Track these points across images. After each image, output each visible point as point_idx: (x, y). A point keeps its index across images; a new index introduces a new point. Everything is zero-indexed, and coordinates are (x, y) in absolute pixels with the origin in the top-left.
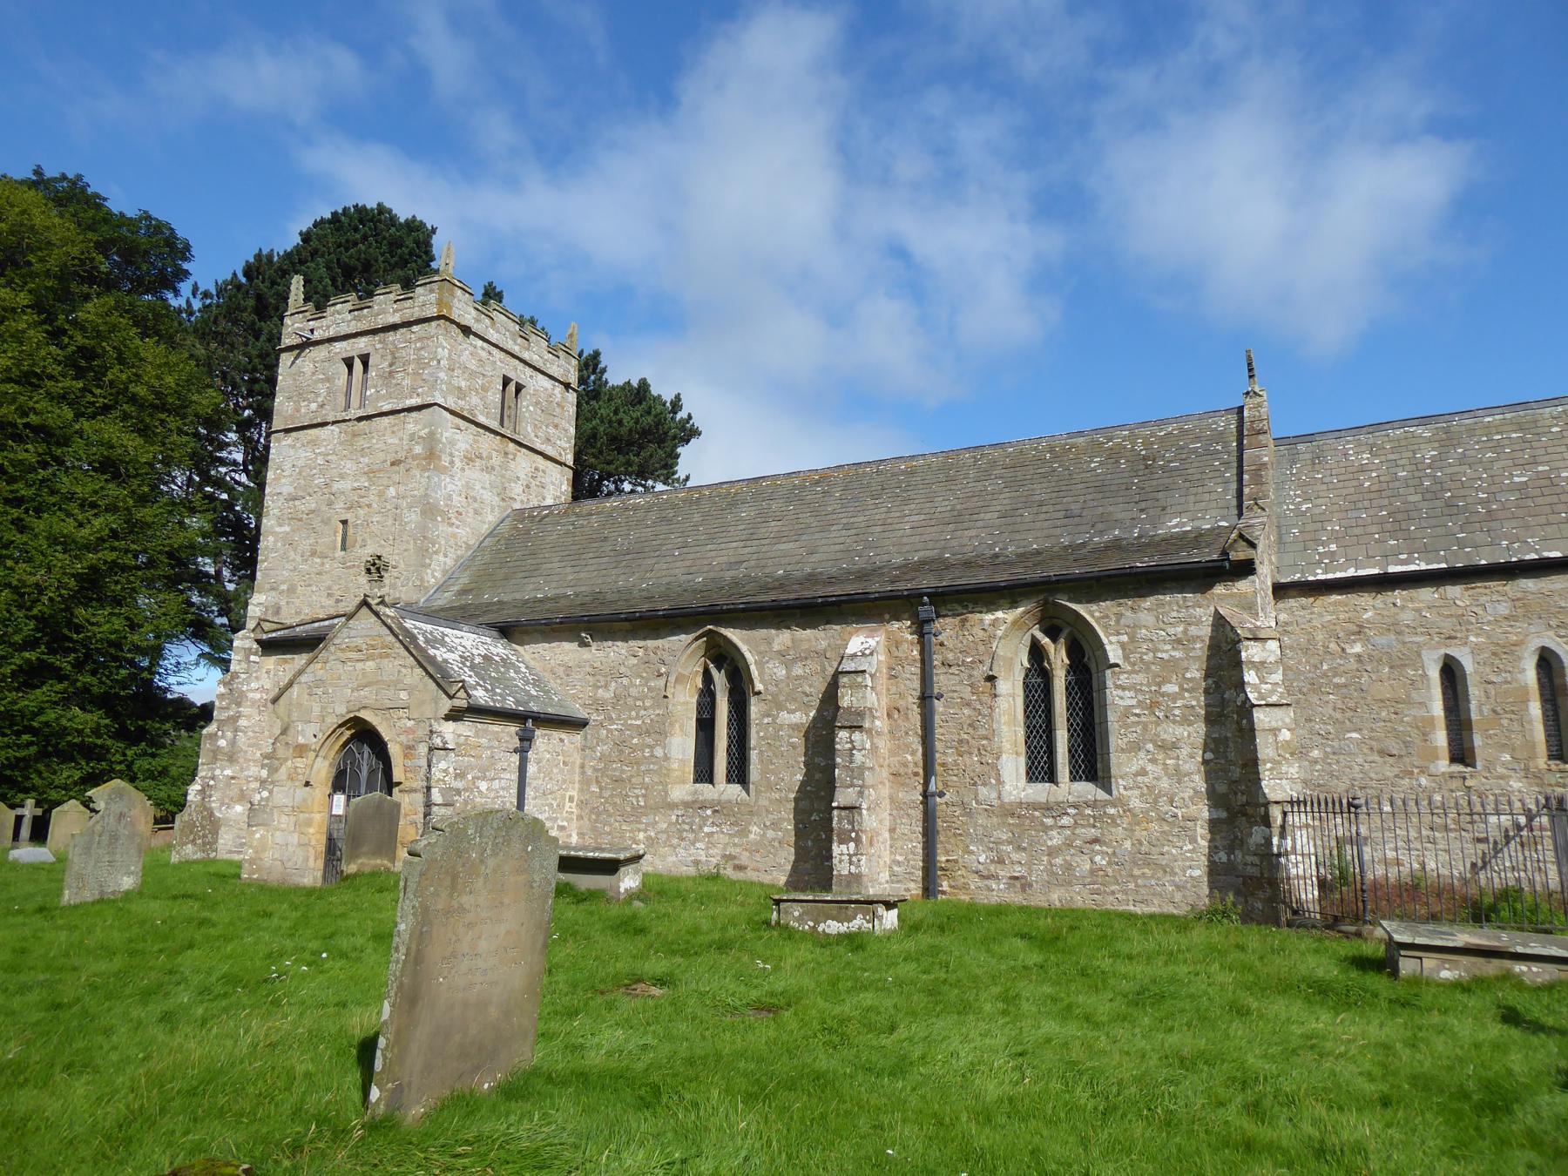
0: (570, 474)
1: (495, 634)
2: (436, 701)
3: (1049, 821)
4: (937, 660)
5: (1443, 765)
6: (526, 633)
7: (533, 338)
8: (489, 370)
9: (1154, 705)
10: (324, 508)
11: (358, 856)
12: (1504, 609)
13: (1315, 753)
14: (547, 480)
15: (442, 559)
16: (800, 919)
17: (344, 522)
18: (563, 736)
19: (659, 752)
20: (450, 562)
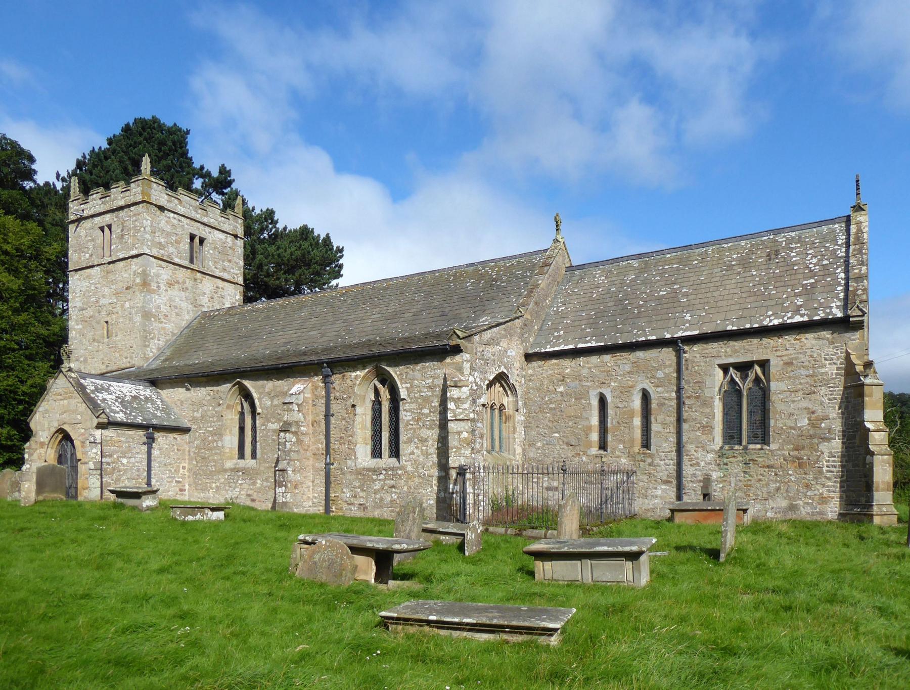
0: (241, 289)
1: (147, 384)
2: (91, 419)
3: (375, 477)
4: (332, 396)
5: (595, 450)
6: (163, 383)
7: (209, 209)
8: (179, 231)
9: (419, 419)
10: (97, 315)
11: (43, 493)
12: (628, 368)
13: (539, 444)
14: (225, 293)
15: (156, 342)
16: (179, 515)
17: (107, 322)
18: (176, 436)
19: (220, 444)
20: (162, 343)
